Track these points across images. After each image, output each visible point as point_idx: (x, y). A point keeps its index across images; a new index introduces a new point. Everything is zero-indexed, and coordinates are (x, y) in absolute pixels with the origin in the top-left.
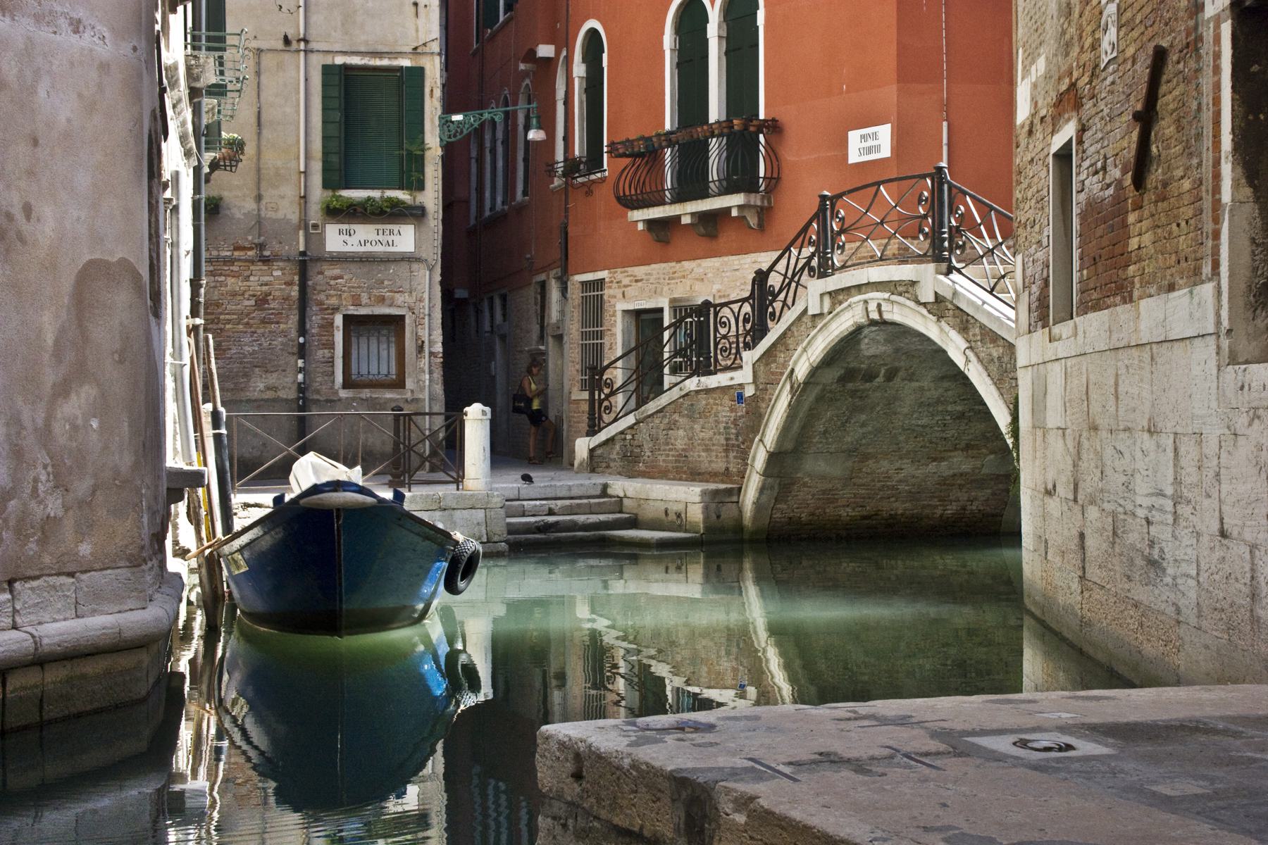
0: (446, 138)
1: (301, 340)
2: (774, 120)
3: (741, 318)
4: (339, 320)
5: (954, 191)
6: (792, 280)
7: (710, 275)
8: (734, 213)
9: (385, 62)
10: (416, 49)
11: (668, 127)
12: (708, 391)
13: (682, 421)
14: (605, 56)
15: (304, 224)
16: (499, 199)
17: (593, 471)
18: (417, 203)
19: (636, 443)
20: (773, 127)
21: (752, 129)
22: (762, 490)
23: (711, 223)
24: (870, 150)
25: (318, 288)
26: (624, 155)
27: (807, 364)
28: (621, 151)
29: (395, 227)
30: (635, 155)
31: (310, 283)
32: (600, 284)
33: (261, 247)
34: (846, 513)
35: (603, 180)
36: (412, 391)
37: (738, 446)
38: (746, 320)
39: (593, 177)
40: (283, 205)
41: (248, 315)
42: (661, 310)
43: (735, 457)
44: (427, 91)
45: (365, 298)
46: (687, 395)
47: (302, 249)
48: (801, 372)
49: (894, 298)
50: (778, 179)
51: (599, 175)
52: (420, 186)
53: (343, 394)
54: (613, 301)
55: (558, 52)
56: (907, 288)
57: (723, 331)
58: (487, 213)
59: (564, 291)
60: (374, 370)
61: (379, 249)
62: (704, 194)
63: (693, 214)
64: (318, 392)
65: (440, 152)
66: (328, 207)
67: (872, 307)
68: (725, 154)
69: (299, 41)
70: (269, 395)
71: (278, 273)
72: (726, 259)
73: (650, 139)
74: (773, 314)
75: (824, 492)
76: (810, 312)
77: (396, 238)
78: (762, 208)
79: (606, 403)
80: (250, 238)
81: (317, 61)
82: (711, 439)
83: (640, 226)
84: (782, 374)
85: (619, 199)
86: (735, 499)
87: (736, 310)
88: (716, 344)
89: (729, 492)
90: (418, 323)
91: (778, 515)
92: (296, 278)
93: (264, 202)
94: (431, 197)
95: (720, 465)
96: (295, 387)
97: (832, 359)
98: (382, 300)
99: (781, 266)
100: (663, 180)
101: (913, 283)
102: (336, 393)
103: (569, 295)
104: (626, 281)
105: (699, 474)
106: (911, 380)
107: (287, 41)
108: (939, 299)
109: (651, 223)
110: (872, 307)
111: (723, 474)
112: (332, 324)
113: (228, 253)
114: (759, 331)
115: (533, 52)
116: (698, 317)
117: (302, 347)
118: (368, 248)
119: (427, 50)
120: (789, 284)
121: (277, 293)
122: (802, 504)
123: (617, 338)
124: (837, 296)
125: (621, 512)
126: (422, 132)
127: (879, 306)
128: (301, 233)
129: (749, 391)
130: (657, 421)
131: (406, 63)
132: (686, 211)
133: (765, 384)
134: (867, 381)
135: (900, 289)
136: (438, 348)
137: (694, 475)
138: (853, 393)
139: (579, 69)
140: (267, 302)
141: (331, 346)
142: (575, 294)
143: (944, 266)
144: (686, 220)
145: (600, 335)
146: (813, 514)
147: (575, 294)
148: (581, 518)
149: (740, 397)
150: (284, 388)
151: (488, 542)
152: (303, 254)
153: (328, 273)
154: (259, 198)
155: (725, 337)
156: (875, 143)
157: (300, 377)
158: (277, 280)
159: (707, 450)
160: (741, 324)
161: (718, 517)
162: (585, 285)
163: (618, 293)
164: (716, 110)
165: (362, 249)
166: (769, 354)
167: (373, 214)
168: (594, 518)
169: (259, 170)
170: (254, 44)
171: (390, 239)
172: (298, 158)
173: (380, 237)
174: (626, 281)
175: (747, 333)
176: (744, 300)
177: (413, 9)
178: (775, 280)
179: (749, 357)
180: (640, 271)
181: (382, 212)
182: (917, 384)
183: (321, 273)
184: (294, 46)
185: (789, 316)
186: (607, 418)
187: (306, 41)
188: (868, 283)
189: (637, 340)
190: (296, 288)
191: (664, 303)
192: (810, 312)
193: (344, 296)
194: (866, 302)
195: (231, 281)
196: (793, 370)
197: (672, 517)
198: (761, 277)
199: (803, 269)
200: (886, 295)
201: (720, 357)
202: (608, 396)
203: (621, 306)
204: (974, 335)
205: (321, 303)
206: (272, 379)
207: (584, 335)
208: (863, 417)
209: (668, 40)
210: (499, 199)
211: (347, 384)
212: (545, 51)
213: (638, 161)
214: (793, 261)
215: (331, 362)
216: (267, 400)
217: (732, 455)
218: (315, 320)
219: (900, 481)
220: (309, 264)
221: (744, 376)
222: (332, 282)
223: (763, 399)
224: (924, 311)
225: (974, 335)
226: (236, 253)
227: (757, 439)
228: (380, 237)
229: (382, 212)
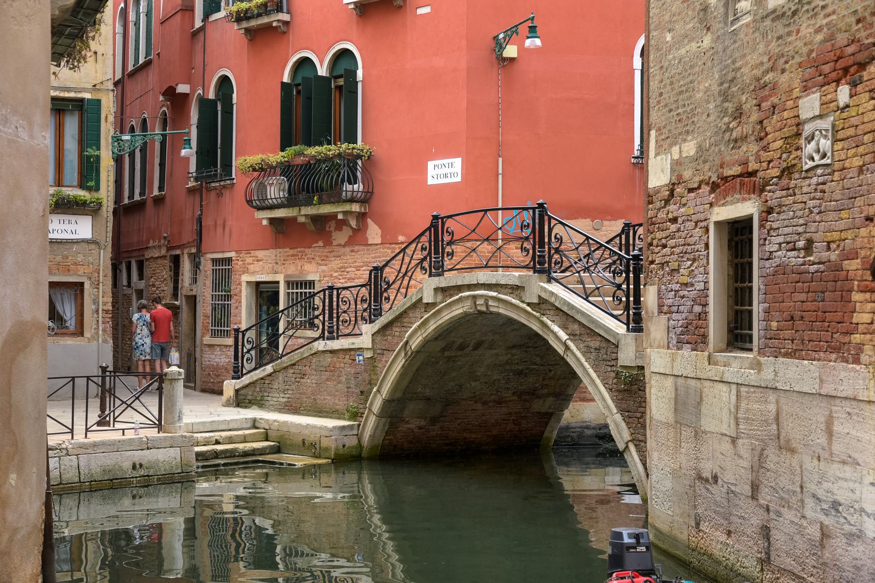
0: (116, 150)
3: (359, 299)
5: (553, 222)
8: (340, 217)
9: (72, 95)
10: (94, 86)
12: (332, 352)
16: (137, 191)
17: (238, 405)
32: (229, 260)
42: (278, 282)
46: (315, 353)
51: (229, 182)
55: (193, 90)
57: (344, 307)
58: (126, 201)
59: (196, 266)
63: (306, 216)
76: (425, 301)
83: (265, 222)
84: (398, 344)
88: (338, 318)
94: (106, 193)
106: (491, 349)
109: (272, 221)
119: (103, 87)
124: (445, 291)
125: (267, 440)
131: (87, 96)
133: (380, 350)
143: (544, 276)
145: (228, 297)
147: (207, 266)
148: (241, 446)
155: (317, 317)
168: (248, 446)
176: (362, 286)
178: (390, 274)
182: (495, 351)
185: (401, 303)
191: (280, 278)
192: (425, 301)
194: (475, 297)
201: (341, 327)
203: (245, 278)
210: (137, 191)
214: (407, 260)
227: (375, 390)
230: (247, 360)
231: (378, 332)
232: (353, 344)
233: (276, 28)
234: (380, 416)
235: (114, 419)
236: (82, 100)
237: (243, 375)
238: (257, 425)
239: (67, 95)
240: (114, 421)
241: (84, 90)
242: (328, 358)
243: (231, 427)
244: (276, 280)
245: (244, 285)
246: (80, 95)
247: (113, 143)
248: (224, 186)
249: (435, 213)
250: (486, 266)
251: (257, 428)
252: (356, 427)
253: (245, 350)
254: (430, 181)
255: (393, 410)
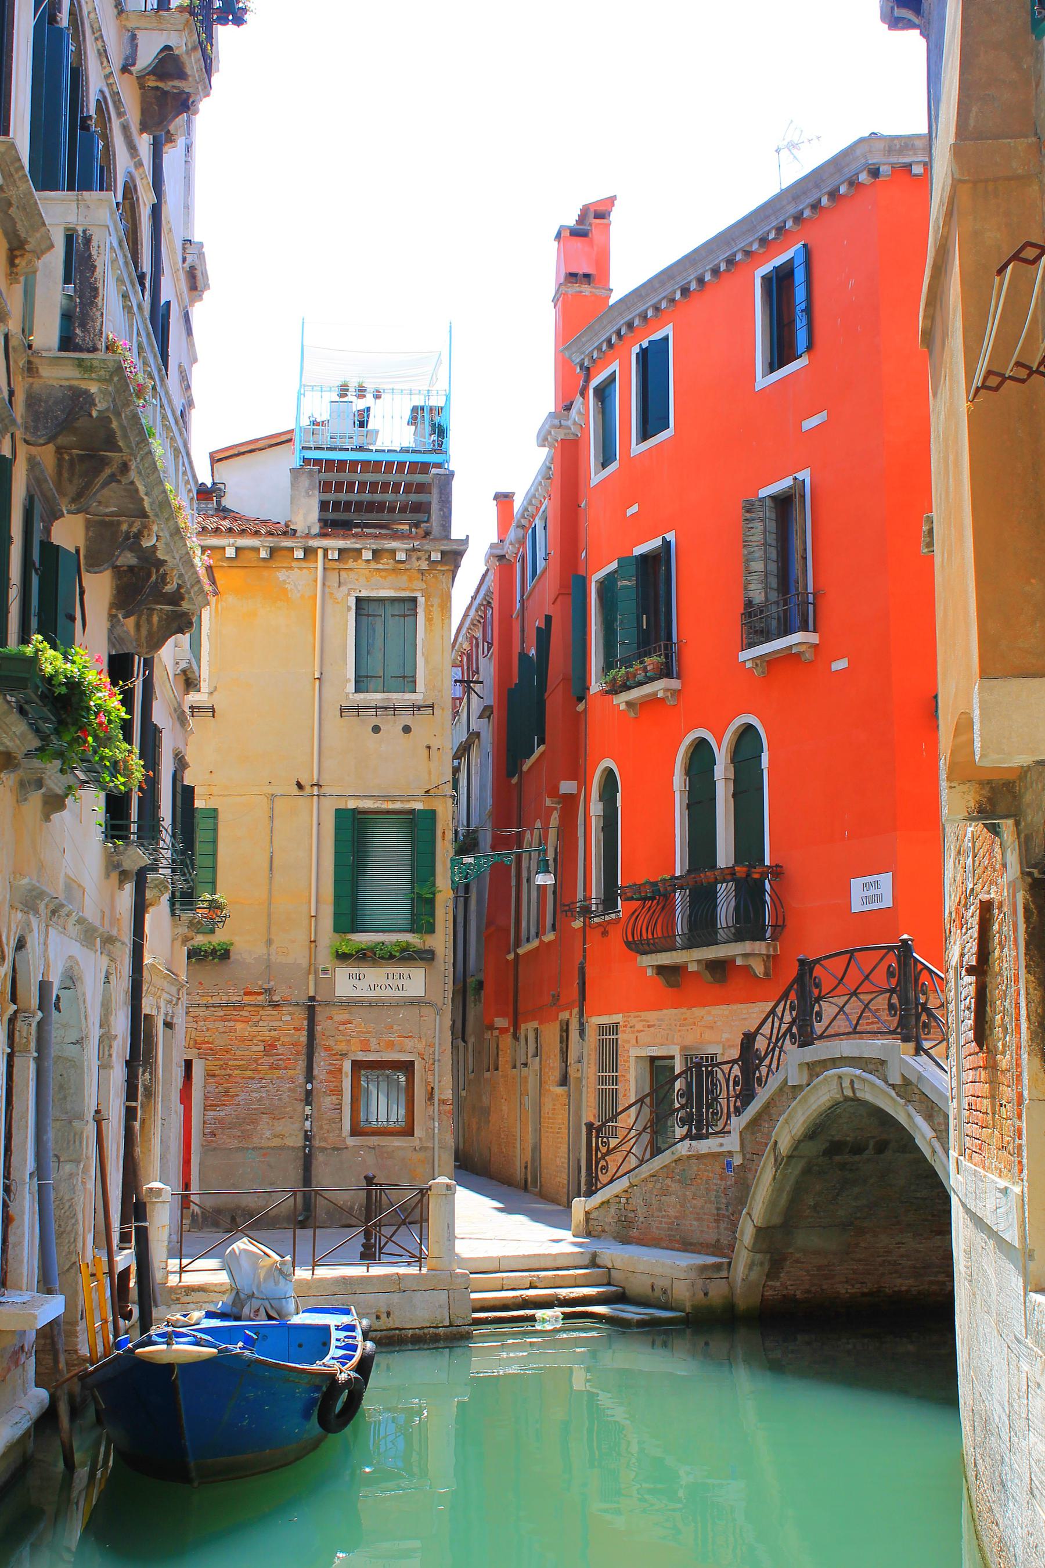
1: (309, 1086)
2: (777, 866)
4: (347, 1066)
6: (775, 1044)
7: (719, 1023)
9: (397, 806)
10: (427, 792)
11: (678, 874)
12: (699, 1157)
13: (675, 1186)
14: (619, 795)
15: (312, 968)
18: (427, 947)
19: (630, 1207)
20: (777, 871)
21: (756, 876)
22: (751, 1266)
23: (719, 968)
24: (872, 900)
25: (327, 1033)
26: (632, 899)
27: (789, 1137)
28: (629, 894)
29: (405, 971)
30: (644, 899)
31: (319, 1028)
32: (614, 1028)
33: (269, 991)
34: (844, 1290)
35: (618, 921)
36: (420, 1139)
37: (728, 1217)
38: (736, 1083)
39: (607, 918)
40: (291, 949)
41: (256, 1061)
43: (726, 1229)
44: (439, 833)
45: (373, 1044)
47: (311, 994)
48: (785, 1146)
49: (865, 1075)
50: (784, 926)
51: (613, 916)
52: (431, 930)
53: (351, 1141)
54: (627, 1046)
56: (876, 1066)
60: (383, 1117)
61: (389, 993)
62: (712, 941)
63: (699, 961)
64: (325, 1140)
65: (451, 894)
66: (337, 952)
67: (846, 1083)
68: (733, 903)
69: (312, 785)
70: (276, 1142)
71: (288, 1018)
72: (734, 1007)
73: (655, 884)
74: (759, 1079)
75: (820, 1268)
77: (406, 982)
78: (768, 956)
79: (602, 1163)
80: (260, 983)
81: (330, 807)
82: (702, 1207)
83: (649, 972)
84: (766, 1145)
85: (628, 944)
86: (724, 1274)
87: (727, 1071)
89: (718, 1267)
90: (429, 1069)
91: (770, 1292)
92: (305, 1023)
93: (274, 946)
94: (441, 941)
95: (711, 1237)
96: (302, 1135)
97: (814, 1132)
98: (391, 1045)
99: (766, 1030)
100: (673, 924)
101: (883, 1062)
102: (344, 1141)
103: (586, 1038)
104: (639, 1026)
105: (691, 1244)
107: (300, 786)
108: (907, 1082)
109: (661, 970)
110: (846, 1083)
111: (714, 1246)
112: (340, 1070)
113: (239, 998)
114: (746, 1096)
115: (556, 788)
116: (701, 1068)
117: (309, 1093)
118: (378, 993)
120: (773, 1050)
121: (287, 1039)
122: (794, 1281)
123: (632, 1083)
124: (814, 1068)
125: (609, 1284)
126: (433, 874)
127: (852, 1082)
128: (311, 977)
129: (737, 1161)
130: (650, 1185)
131: (418, 806)
132: (692, 958)
134: (855, 1154)
135: (871, 1067)
136: (448, 1094)
137: (686, 1246)
138: (843, 1166)
139: (596, 808)
140: (274, 1047)
141: (339, 1092)
142: (592, 1037)
143: (911, 1046)
144: (693, 968)
145: (615, 1080)
146: (808, 1291)
149: (729, 1164)
150: (291, 1135)
151: (451, 1325)
152: (312, 999)
153: (336, 1018)
154: (269, 942)
156: (877, 892)
157: (308, 1124)
158: (287, 1026)
159: (698, 1219)
160: (731, 1088)
161: (706, 1294)
162: (603, 1029)
163: (632, 1037)
164: (725, 855)
165: (372, 993)
166: (754, 1123)
167: (382, 958)
169: (269, 915)
170: (270, 790)
171: (400, 983)
172: (310, 902)
173: (390, 982)
174: (639, 1026)
175: (737, 1096)
176: (734, 1062)
177: (426, 751)
179: (738, 1123)
180: (652, 1016)
181: (392, 957)
183: (331, 1018)
184: (308, 790)
185: (773, 1083)
186: (603, 1178)
187: (319, 786)
188: (841, 1058)
189: (651, 1087)
190: (305, 1033)
191: (675, 1051)
193: (348, 1039)
195: (239, 1026)
196: (776, 1142)
197: (658, 1293)
198: (749, 1039)
199: (784, 1035)
200: (858, 1072)
202: (604, 1156)
203: (634, 1052)
204: (939, 1124)
205: (328, 1049)
206: (280, 1127)
207: (601, 1080)
208: (856, 1190)
209: (679, 781)
211: (354, 1133)
212: (567, 787)
213: (648, 903)
215: (339, 1108)
216: (273, 1148)
217: (723, 1225)
218: (321, 1069)
219: (902, 1256)
220: (318, 1009)
221: (731, 1143)
222: (342, 1028)
223: (750, 1170)
224: (893, 1094)
225: (939, 1124)
226: (246, 998)
228: (390, 982)
229: (392, 957)
230: (602, 1169)
231: (747, 1127)
232: (721, 1145)
233: (663, 699)
234: (754, 1250)
235: (381, 1249)
236: (412, 812)
237: (597, 1190)
238: (599, 1261)
239: (391, 806)
240: (380, 1253)
241: (413, 797)
242: (694, 1166)
243: (559, 1264)
244: (671, 1054)
245: (632, 1060)
246: (408, 806)
247: (452, 868)
248: (609, 922)
249: (801, 957)
250: (855, 1032)
251: (599, 1267)
252: (725, 1266)
253: (599, 1155)
254: (856, 907)
255: (773, 1240)
